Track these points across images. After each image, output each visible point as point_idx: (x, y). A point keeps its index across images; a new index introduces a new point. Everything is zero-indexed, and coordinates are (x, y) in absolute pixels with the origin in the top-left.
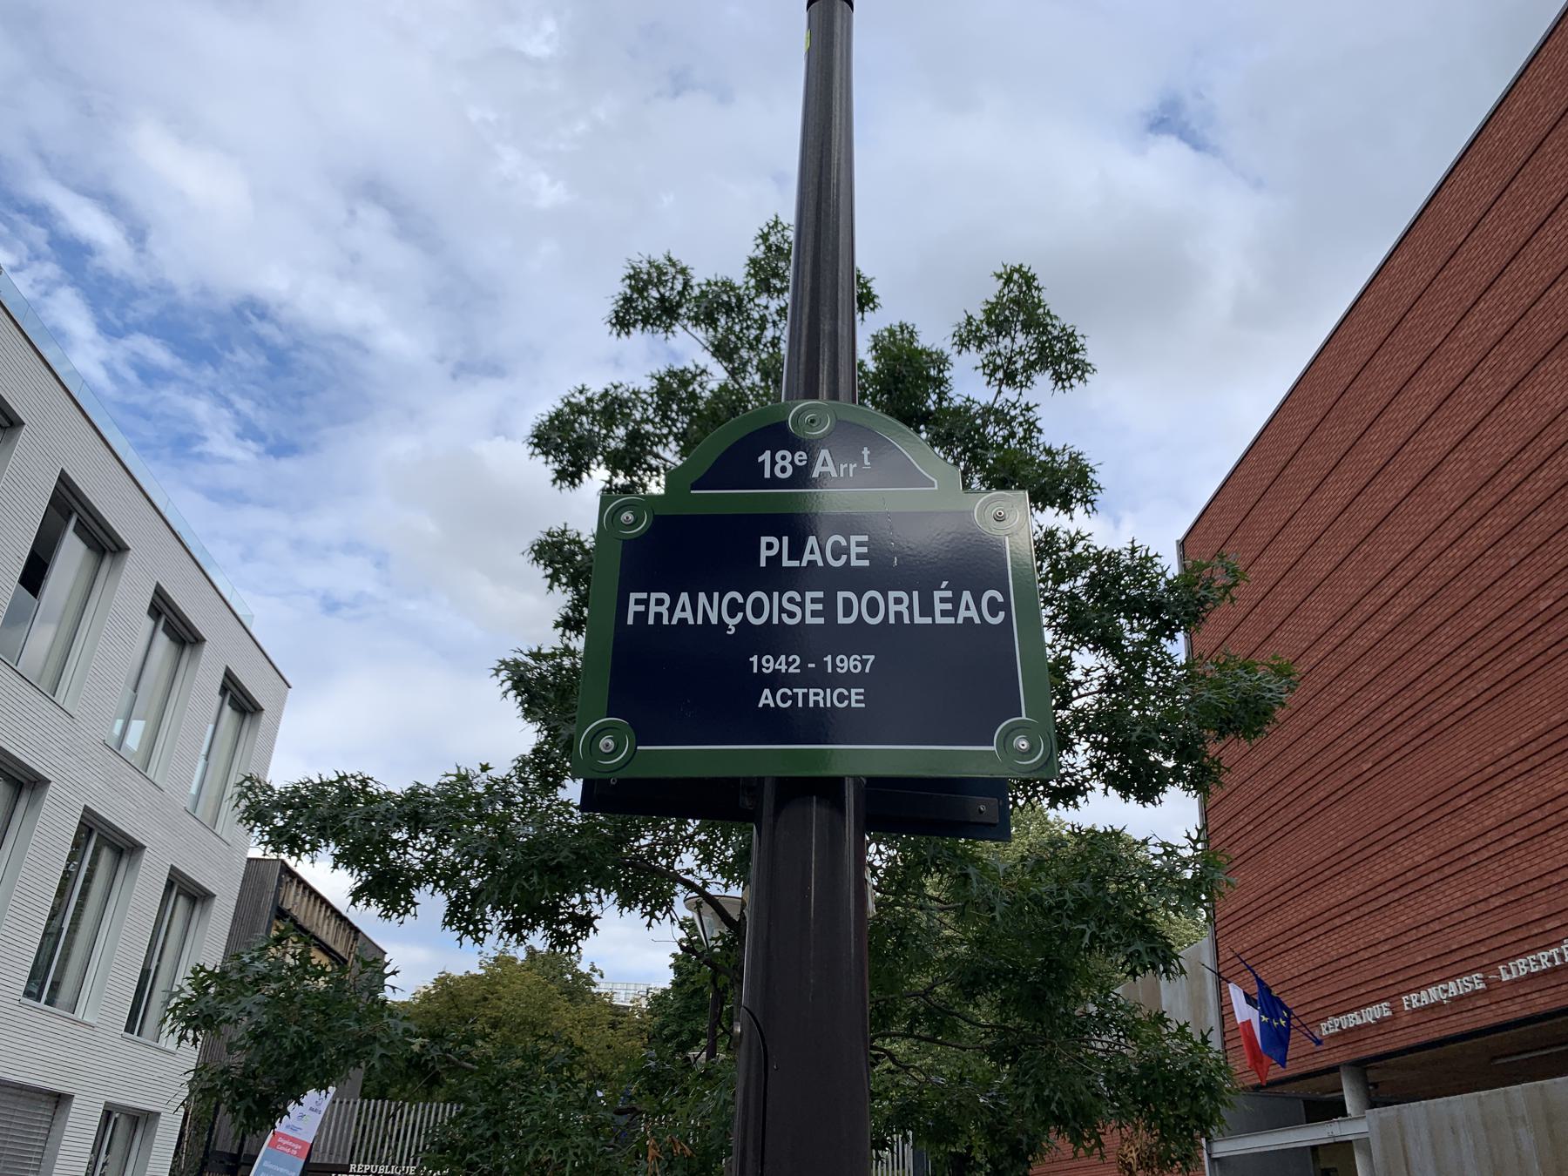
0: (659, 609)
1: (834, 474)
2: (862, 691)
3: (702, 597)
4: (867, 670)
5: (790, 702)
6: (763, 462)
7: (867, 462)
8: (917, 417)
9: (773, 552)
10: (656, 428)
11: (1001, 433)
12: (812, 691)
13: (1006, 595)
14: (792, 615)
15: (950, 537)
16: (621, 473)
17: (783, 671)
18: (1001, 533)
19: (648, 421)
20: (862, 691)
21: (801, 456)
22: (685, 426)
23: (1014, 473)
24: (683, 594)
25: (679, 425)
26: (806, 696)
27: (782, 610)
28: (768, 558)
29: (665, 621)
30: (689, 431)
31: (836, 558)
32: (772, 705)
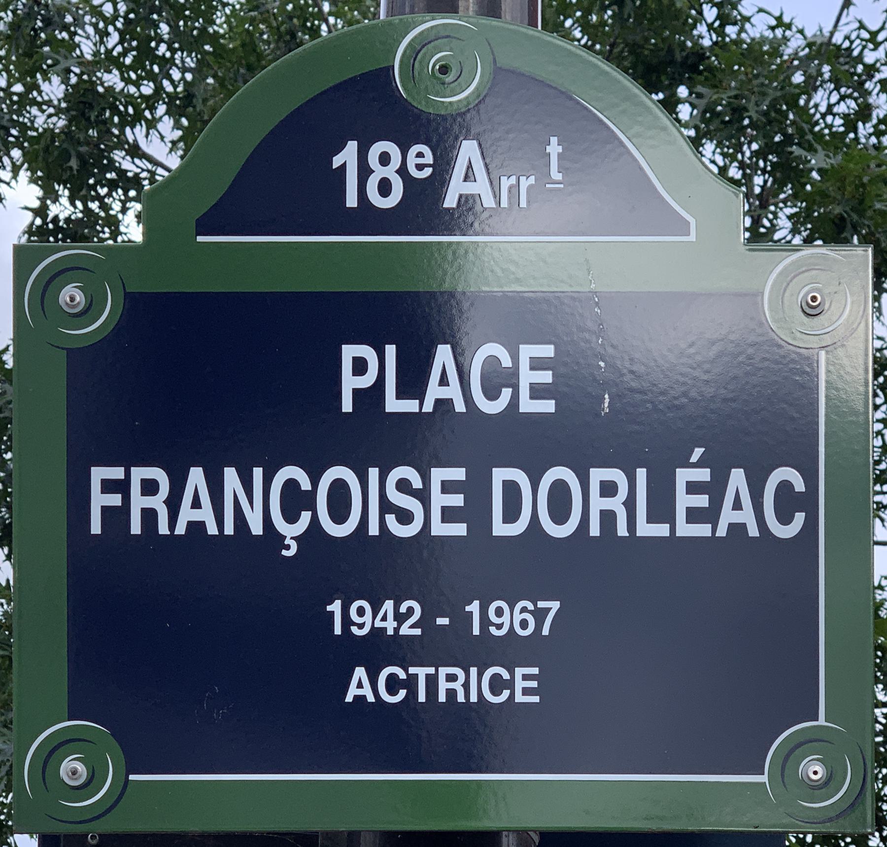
0: (608, 503)
1: (488, 201)
2: (535, 671)
3: (231, 476)
4: (546, 631)
5: (402, 693)
6: (343, 167)
7: (556, 175)
8: (672, 62)
9: (367, 381)
10: (127, 81)
11: (842, 108)
12: (443, 671)
13: (810, 478)
14: (405, 517)
15: (715, 349)
16: (64, 193)
17: (390, 632)
18: (814, 343)
19: (110, 61)
20: (535, 671)
21: (420, 155)
22: (189, 77)
23: (860, 205)
24: (193, 470)
25: (176, 74)
26: (432, 681)
27: (386, 506)
28: (357, 393)
29: (163, 529)
30: (199, 92)
31: (491, 394)
32: (371, 698)
